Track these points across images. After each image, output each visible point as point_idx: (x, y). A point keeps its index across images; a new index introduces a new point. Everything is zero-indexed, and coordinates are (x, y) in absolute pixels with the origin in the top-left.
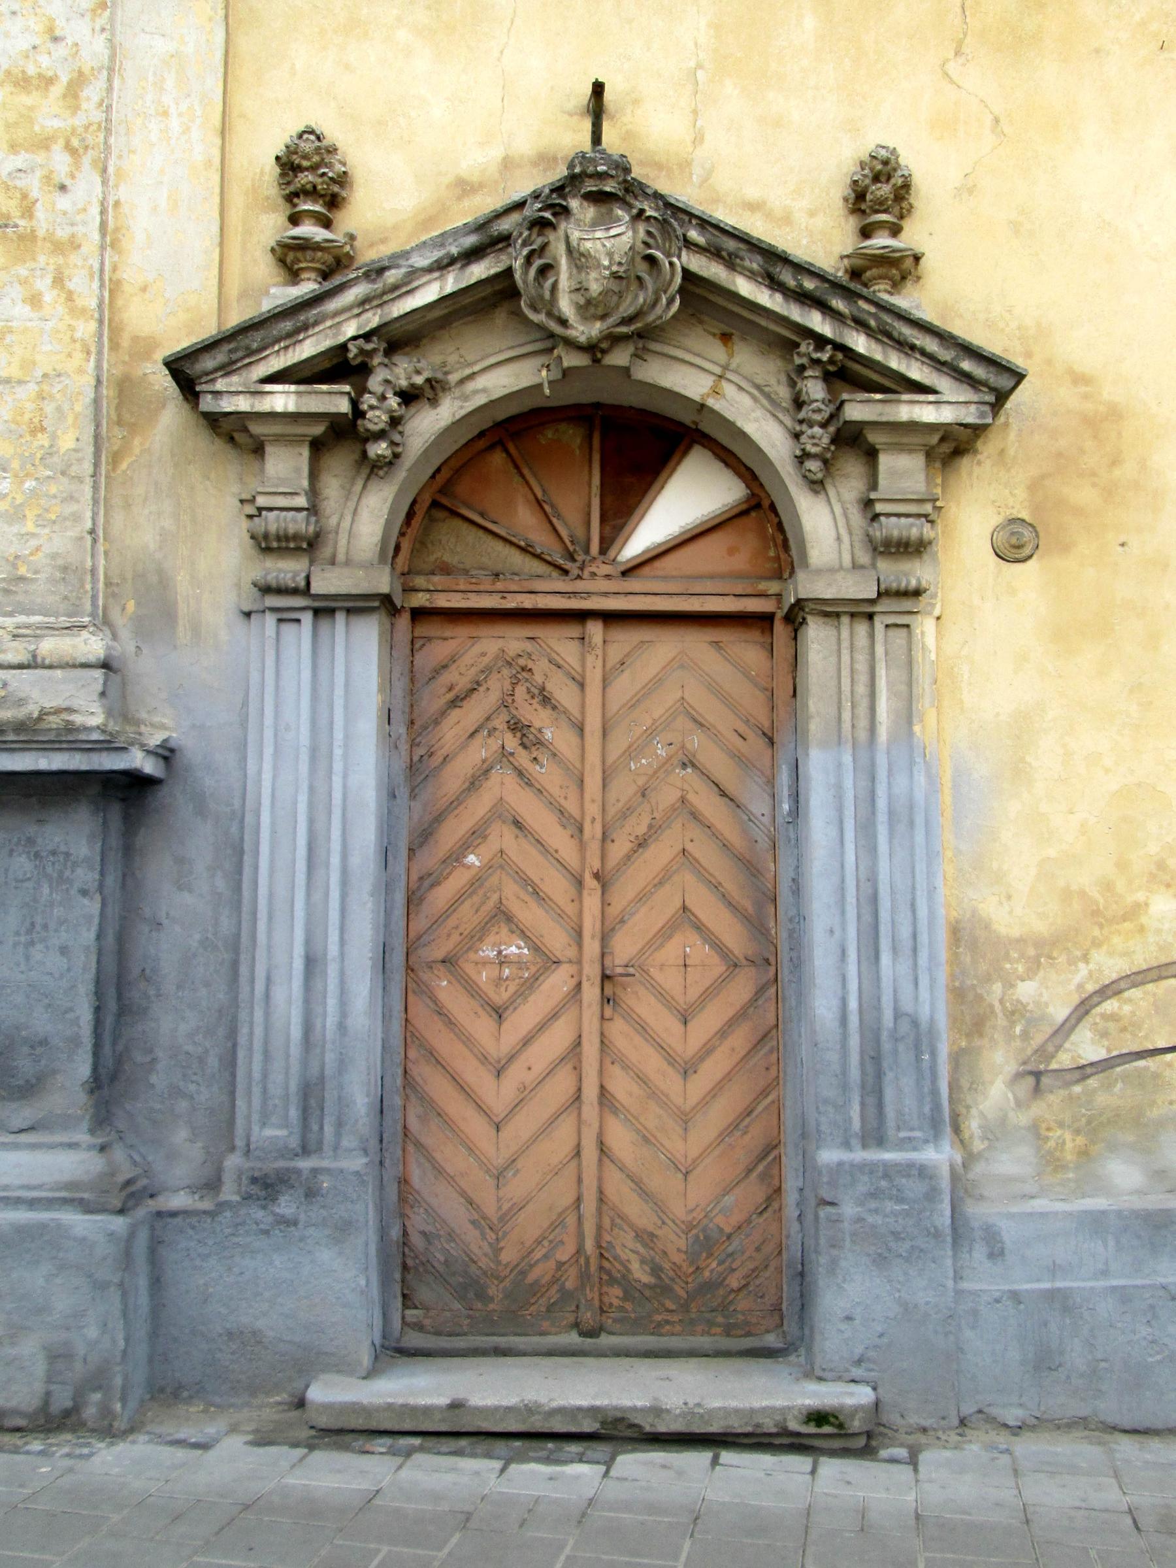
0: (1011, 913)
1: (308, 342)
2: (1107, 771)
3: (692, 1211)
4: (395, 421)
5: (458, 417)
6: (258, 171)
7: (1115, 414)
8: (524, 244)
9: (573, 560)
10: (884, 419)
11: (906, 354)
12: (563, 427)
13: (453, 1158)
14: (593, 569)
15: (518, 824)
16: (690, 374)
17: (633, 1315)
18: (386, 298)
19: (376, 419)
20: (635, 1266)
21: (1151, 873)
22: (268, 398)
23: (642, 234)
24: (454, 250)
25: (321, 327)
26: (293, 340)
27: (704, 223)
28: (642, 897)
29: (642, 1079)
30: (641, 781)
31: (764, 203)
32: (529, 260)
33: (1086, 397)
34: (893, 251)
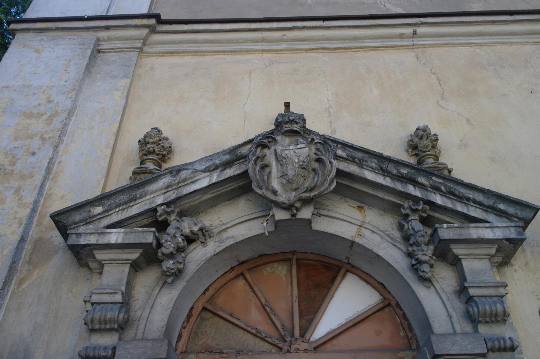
1: (135, 207)
4: (180, 250)
5: (217, 251)
6: (131, 150)
8: (253, 155)
9: (285, 341)
10: (463, 237)
11: (465, 203)
12: (276, 265)
14: (296, 346)
16: (344, 222)
18: (180, 185)
19: (169, 247)
22: (108, 236)
23: (314, 150)
24: (218, 162)
25: (143, 199)
26: (127, 206)
27: (345, 145)
32: (255, 163)
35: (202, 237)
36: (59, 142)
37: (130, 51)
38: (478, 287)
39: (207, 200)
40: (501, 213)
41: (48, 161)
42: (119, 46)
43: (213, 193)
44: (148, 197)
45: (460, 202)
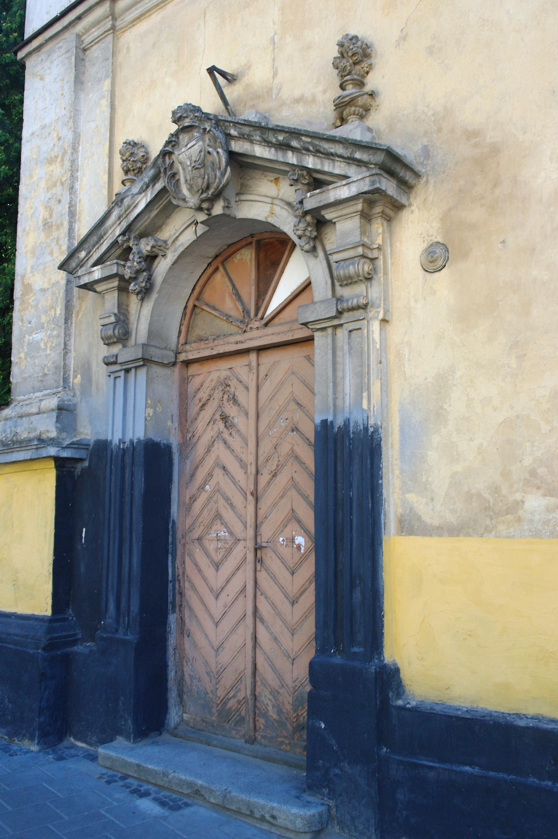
0: (433, 510)
1: (105, 243)
2: (495, 409)
3: (295, 681)
7: (495, 150)
10: (322, 204)
13: (198, 636)
15: (224, 468)
17: (269, 736)
18: (127, 213)
20: (270, 708)
21: (526, 479)
22: (94, 274)
28: (275, 504)
29: (273, 606)
30: (274, 441)
31: (303, 96)
33: (476, 145)
34: (344, 98)
35: (160, 251)
36: (73, 182)
37: (106, 37)
38: (338, 252)
39: (157, 215)
40: (360, 163)
41: (68, 206)
42: (96, 34)
43: (157, 208)
44: (110, 232)
45: (328, 159)
